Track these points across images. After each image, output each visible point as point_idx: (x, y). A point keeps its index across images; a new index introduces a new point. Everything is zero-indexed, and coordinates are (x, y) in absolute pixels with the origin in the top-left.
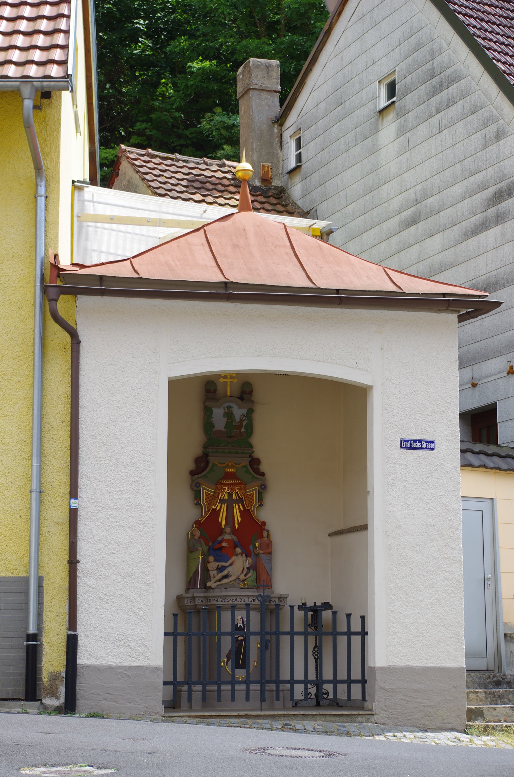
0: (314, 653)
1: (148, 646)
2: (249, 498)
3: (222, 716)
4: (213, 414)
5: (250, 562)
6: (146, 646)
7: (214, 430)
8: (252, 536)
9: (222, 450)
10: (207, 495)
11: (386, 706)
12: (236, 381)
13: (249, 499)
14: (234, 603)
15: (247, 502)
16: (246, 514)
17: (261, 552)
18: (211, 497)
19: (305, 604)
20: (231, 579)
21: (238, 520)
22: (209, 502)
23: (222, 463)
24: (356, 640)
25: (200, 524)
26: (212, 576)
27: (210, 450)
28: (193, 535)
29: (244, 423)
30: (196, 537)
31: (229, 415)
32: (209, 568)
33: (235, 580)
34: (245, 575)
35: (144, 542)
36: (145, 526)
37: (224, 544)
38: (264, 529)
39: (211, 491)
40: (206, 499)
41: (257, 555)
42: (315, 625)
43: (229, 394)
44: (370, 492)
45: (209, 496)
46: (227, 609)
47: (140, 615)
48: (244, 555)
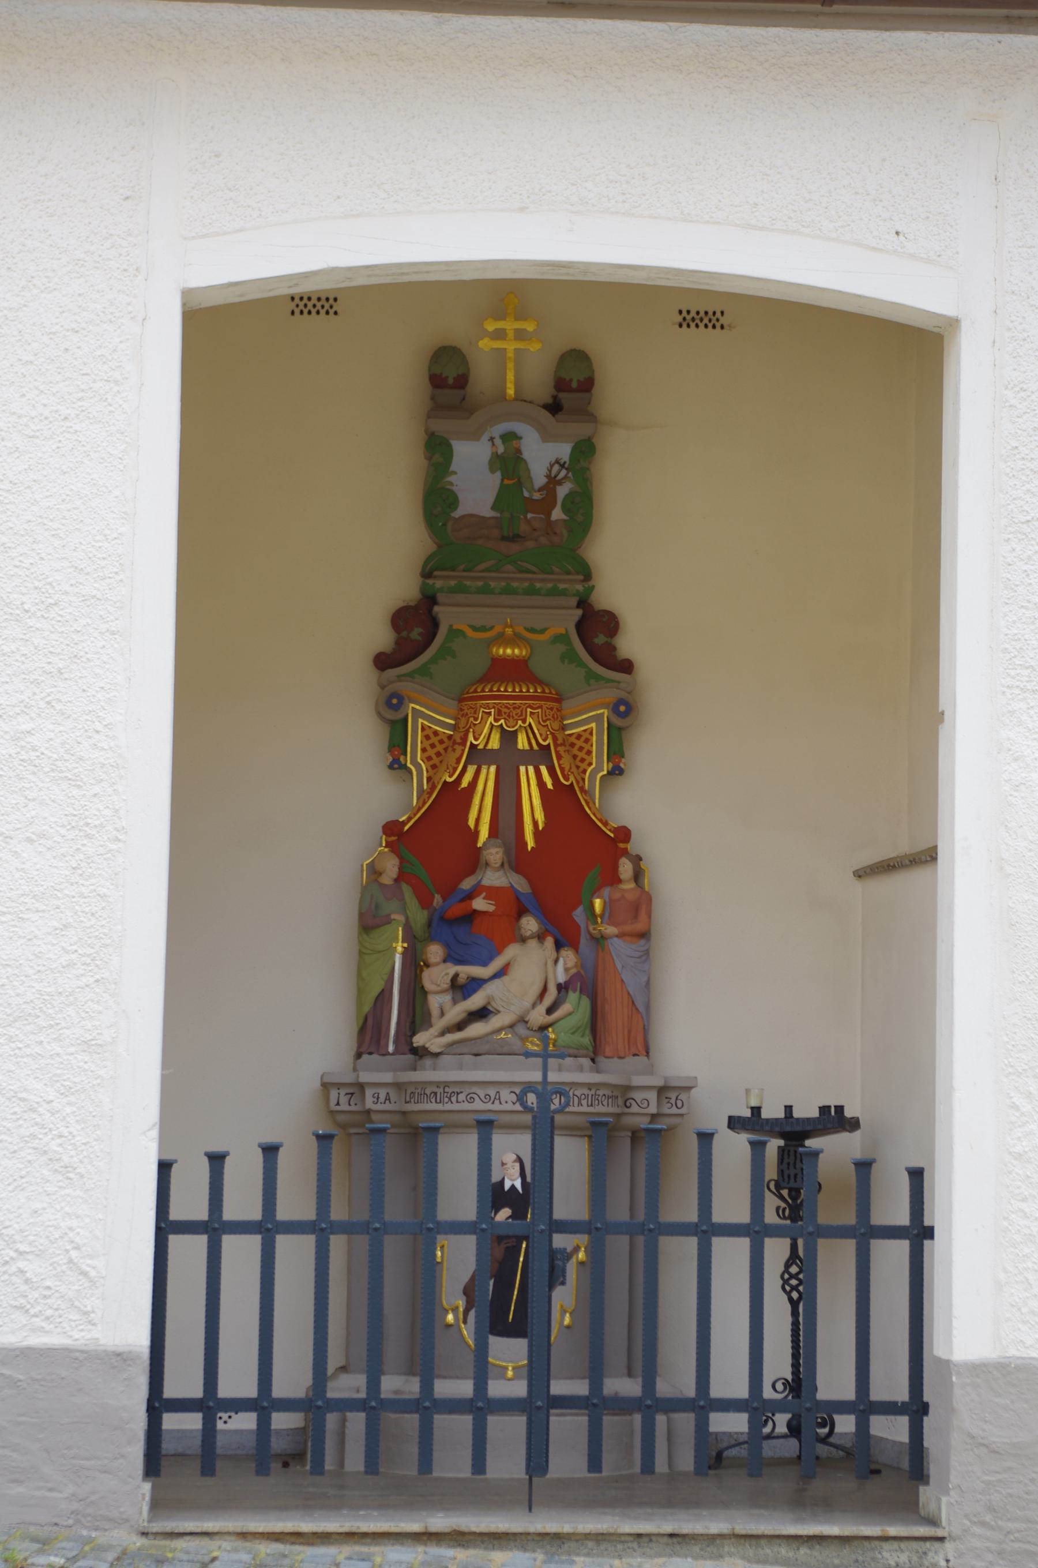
0: (785, 1282)
1: (93, 1273)
2: (573, 745)
3: (365, 1535)
4: (455, 458)
5: (570, 964)
6: (84, 1274)
7: (457, 514)
8: (581, 876)
9: (480, 584)
10: (427, 737)
11: (991, 1509)
12: (535, 347)
13: (575, 751)
14: (489, 1106)
15: (566, 761)
16: (561, 800)
17: (611, 930)
18: (441, 742)
19: (756, 1111)
20: (495, 1022)
21: (535, 823)
22: (436, 760)
23: (483, 629)
24: (891, 1257)
25: (401, 835)
26: (435, 1012)
27: (439, 584)
28: (375, 872)
29: (562, 491)
30: (387, 879)
31: (509, 463)
32: (428, 985)
33: (512, 1026)
34: (550, 1011)
35: (82, 895)
36: (88, 836)
37: (480, 904)
38: (625, 852)
39: (443, 722)
40: (424, 750)
41: (599, 940)
42: (792, 1184)
43: (511, 392)
44: (946, 717)
45: (434, 740)
46: (457, 1127)
47: (66, 1160)
48: (550, 941)
